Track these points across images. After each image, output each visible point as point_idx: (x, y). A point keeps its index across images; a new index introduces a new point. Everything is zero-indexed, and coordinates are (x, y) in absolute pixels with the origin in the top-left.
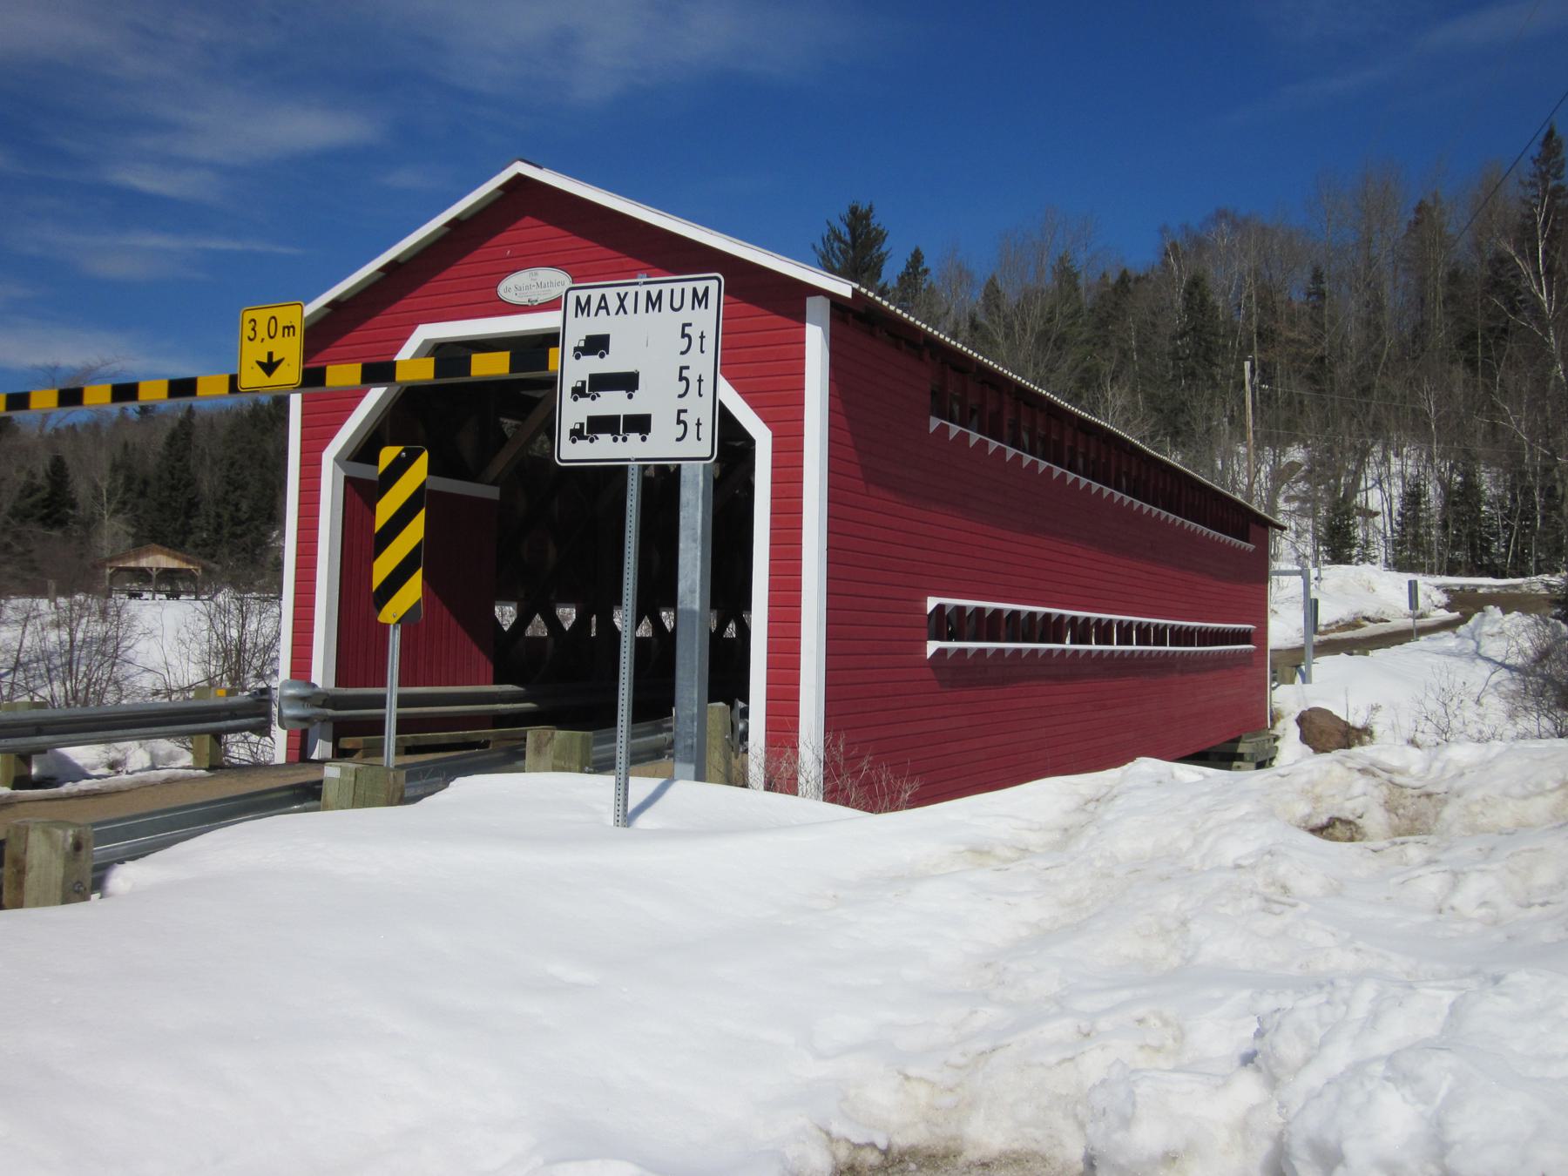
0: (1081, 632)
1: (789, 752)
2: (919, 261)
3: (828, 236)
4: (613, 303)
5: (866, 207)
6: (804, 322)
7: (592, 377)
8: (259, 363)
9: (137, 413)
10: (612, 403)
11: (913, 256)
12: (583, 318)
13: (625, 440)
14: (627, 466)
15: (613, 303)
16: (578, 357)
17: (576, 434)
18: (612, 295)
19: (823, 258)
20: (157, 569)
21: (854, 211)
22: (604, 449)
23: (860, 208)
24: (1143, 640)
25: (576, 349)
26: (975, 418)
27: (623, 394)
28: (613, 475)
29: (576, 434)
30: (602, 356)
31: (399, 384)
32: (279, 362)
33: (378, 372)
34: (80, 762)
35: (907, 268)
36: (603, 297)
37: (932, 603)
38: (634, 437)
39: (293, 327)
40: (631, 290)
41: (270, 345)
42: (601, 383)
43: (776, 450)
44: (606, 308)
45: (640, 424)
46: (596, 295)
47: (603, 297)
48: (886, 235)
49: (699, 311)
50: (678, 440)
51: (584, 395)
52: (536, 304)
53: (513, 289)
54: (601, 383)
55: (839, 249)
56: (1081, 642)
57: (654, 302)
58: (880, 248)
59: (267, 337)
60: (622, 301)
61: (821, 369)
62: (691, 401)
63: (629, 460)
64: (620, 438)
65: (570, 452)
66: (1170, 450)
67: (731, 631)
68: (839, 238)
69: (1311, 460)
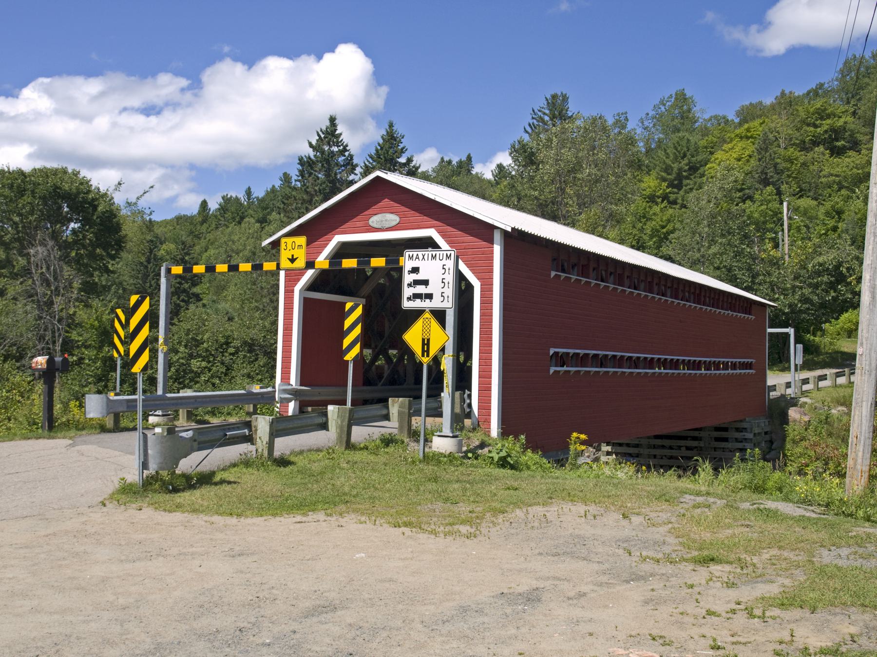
1: (467, 392)
4: (421, 257)
10: (420, 289)
12: (411, 261)
15: (421, 257)
17: (409, 299)
18: (420, 254)
22: (418, 304)
24: (717, 368)
26: (576, 270)
27: (424, 286)
29: (409, 299)
37: (552, 351)
38: (428, 301)
40: (427, 253)
42: (417, 283)
43: (482, 290)
45: (430, 296)
46: (415, 254)
49: (448, 261)
51: (411, 286)
54: (417, 283)
56: (708, 370)
57: (434, 257)
62: (445, 290)
65: (407, 304)
67: (462, 359)
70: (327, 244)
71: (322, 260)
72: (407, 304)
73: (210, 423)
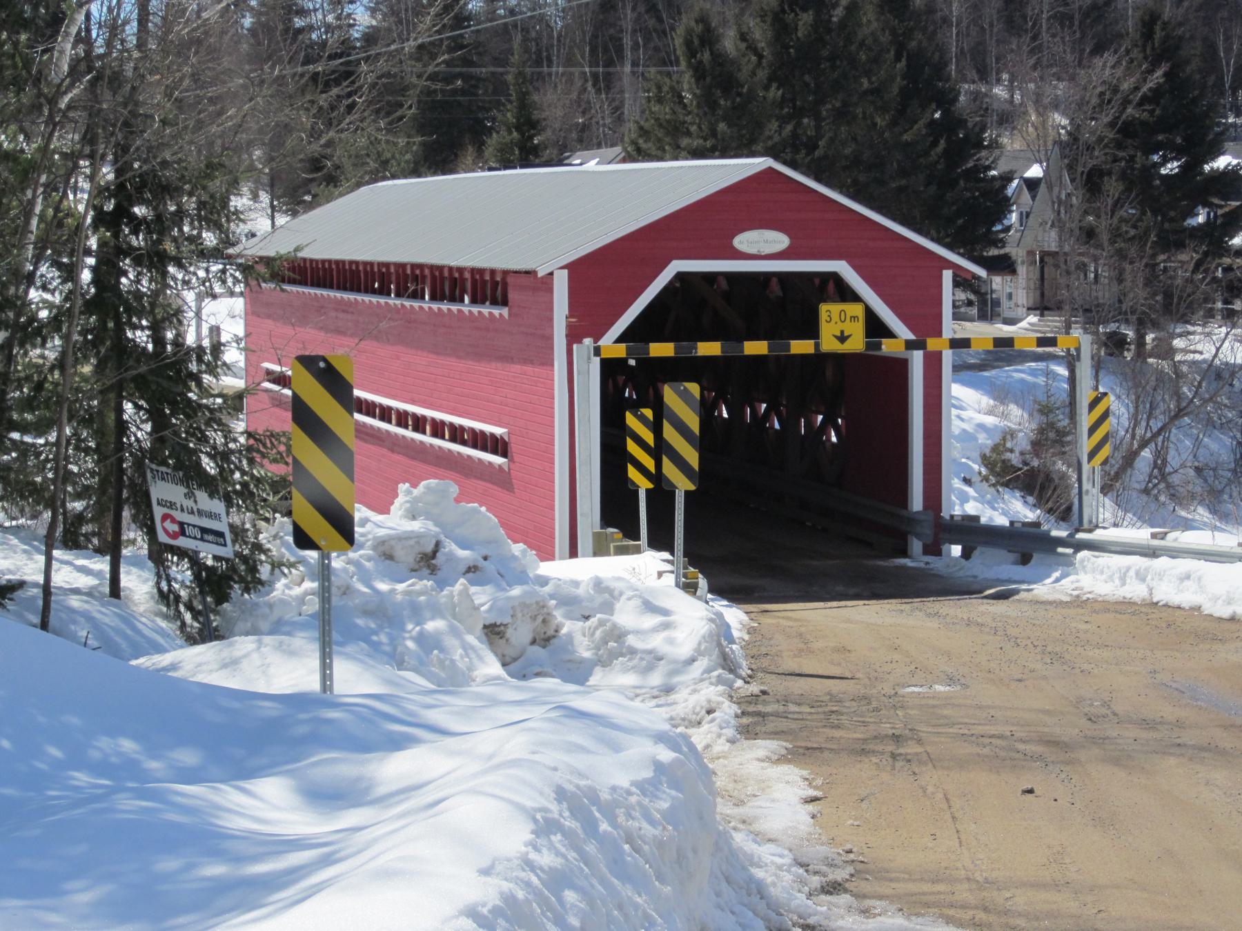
32: (849, 336)
34: (666, 399)
59: (838, 320)
61: (343, 507)
66: (141, 794)
69: (1204, 207)
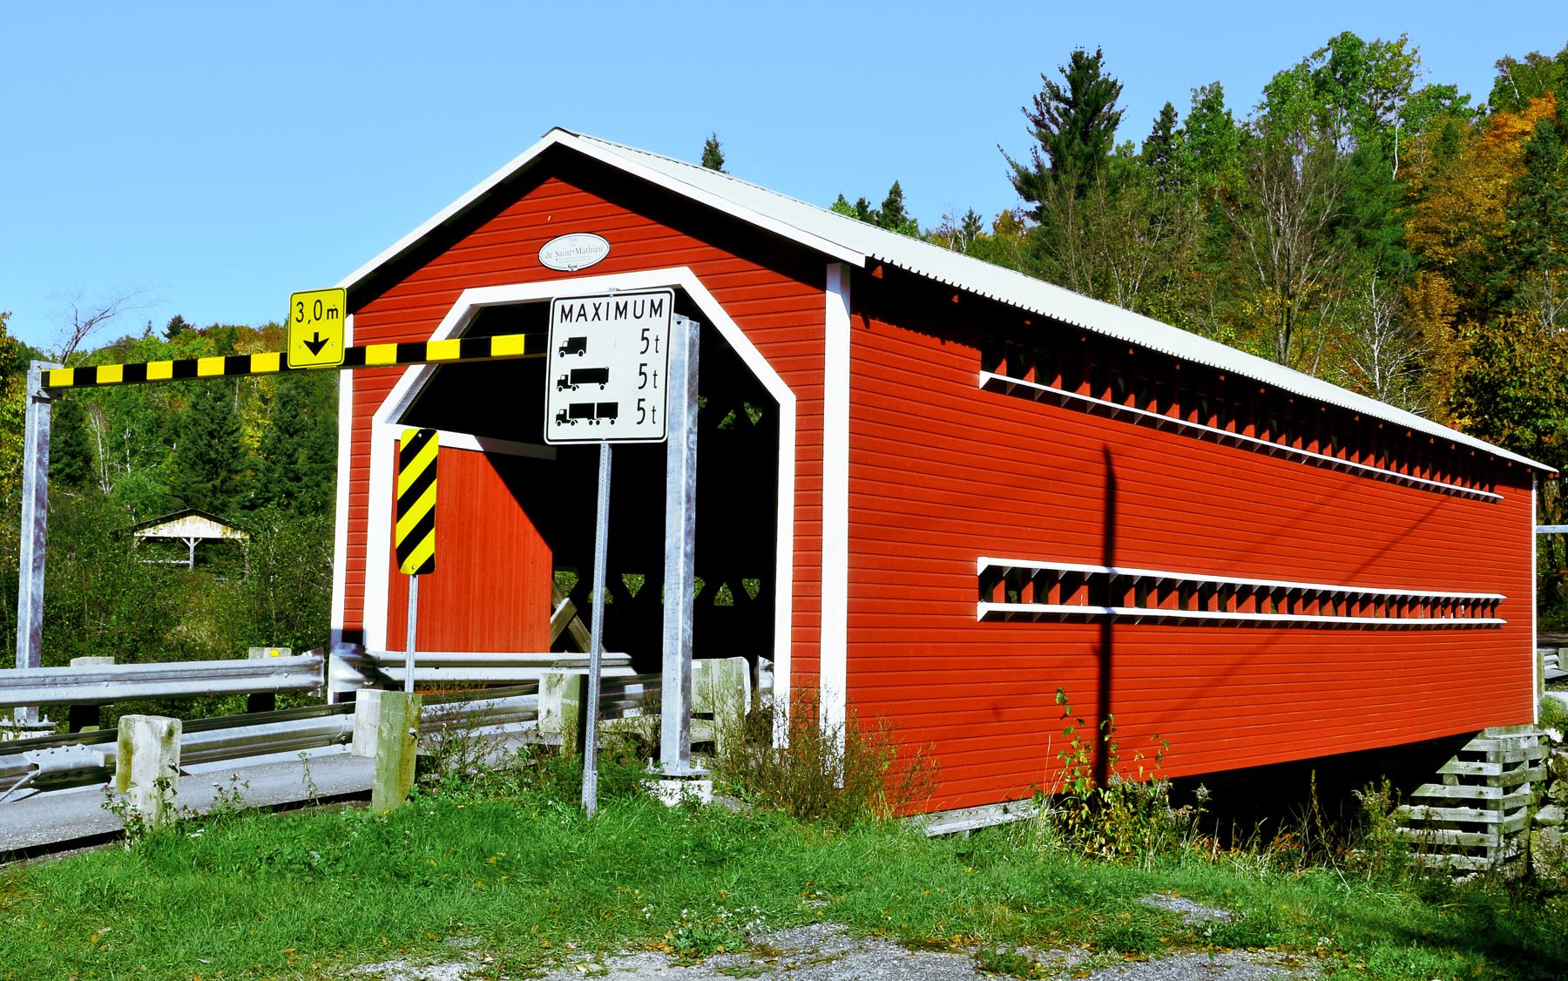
0: (1434, 606)
2: (1171, 121)
3: (1041, 94)
4: (590, 312)
5: (1092, 54)
6: (823, 287)
7: (573, 372)
8: (307, 343)
9: (166, 336)
10: (588, 393)
11: (1163, 113)
13: (598, 423)
14: (599, 445)
15: (590, 312)
16: (562, 355)
17: (561, 418)
19: (1038, 123)
20: (196, 539)
21: (1077, 58)
22: (582, 431)
23: (1085, 55)
25: (561, 349)
27: (597, 385)
28: (587, 454)
29: (561, 418)
30: (581, 354)
31: (432, 363)
33: (412, 352)
35: (1156, 131)
36: (583, 306)
37: (982, 563)
38: (605, 421)
39: (336, 310)
41: (316, 326)
42: (581, 376)
43: (801, 413)
44: (584, 315)
45: (609, 410)
47: (583, 306)
48: (1121, 87)
49: (656, 318)
50: (639, 423)
51: (567, 387)
52: (575, 269)
53: (554, 254)
54: (581, 376)
55: (1057, 108)
58: (1112, 105)
60: (597, 309)
63: (601, 440)
64: (594, 422)
65: (556, 433)
68: (1057, 96)
70: (446, 312)
71: (443, 346)
72: (556, 433)
73: (711, 345)
